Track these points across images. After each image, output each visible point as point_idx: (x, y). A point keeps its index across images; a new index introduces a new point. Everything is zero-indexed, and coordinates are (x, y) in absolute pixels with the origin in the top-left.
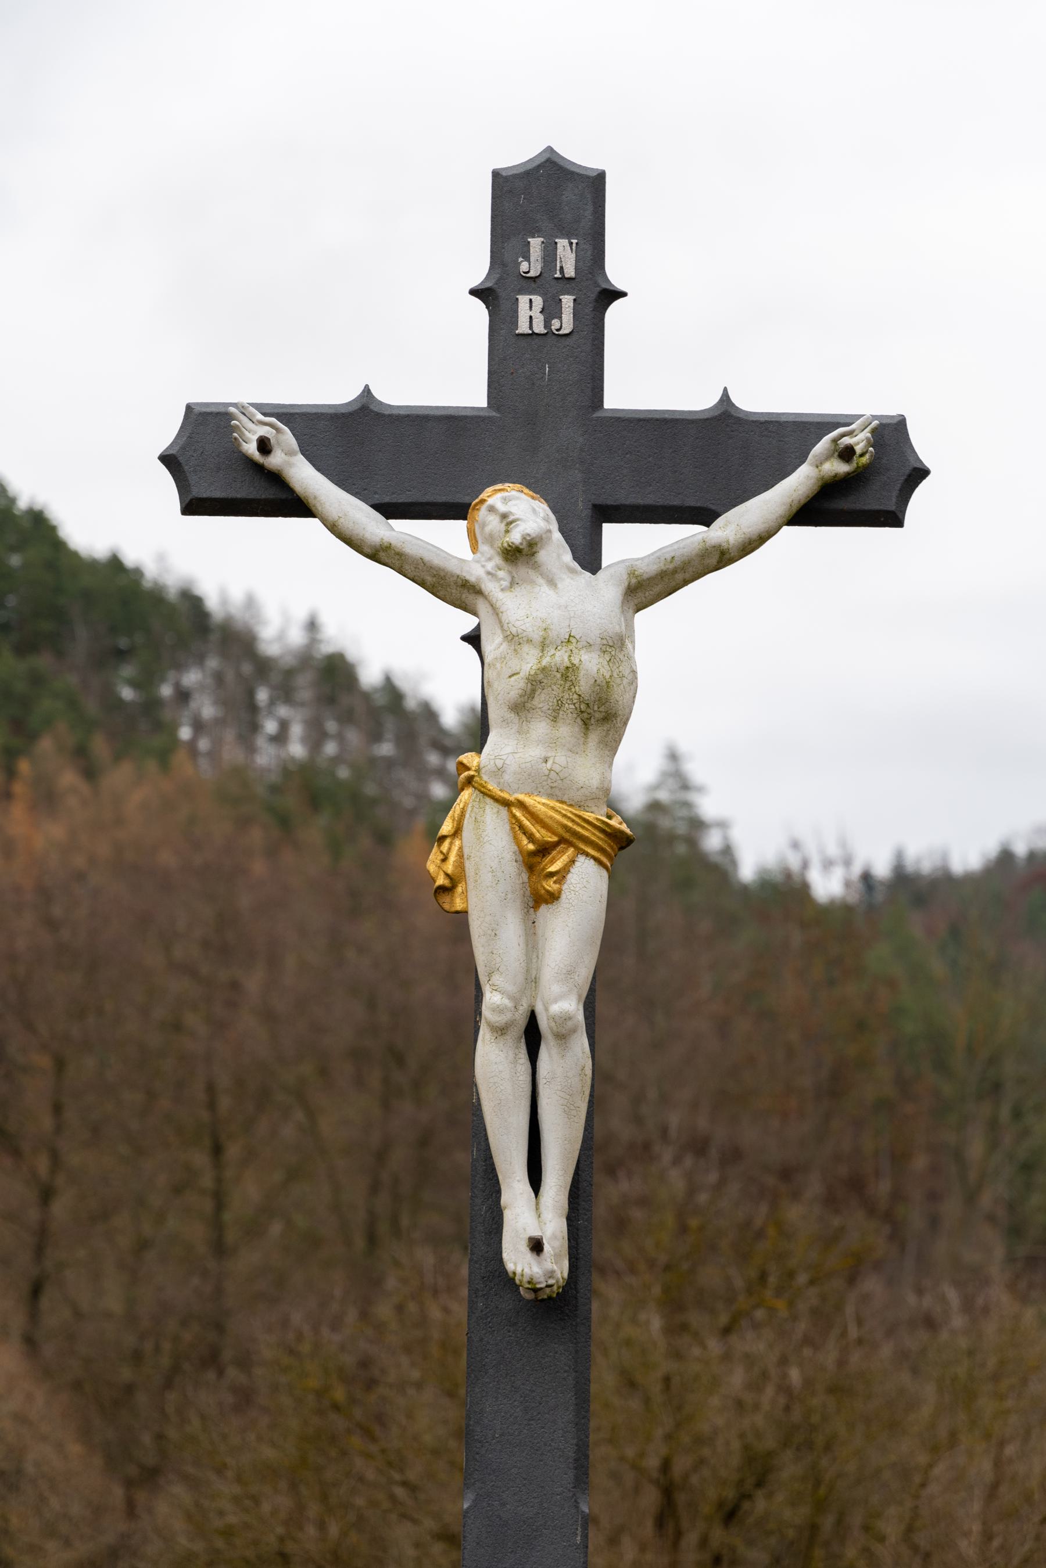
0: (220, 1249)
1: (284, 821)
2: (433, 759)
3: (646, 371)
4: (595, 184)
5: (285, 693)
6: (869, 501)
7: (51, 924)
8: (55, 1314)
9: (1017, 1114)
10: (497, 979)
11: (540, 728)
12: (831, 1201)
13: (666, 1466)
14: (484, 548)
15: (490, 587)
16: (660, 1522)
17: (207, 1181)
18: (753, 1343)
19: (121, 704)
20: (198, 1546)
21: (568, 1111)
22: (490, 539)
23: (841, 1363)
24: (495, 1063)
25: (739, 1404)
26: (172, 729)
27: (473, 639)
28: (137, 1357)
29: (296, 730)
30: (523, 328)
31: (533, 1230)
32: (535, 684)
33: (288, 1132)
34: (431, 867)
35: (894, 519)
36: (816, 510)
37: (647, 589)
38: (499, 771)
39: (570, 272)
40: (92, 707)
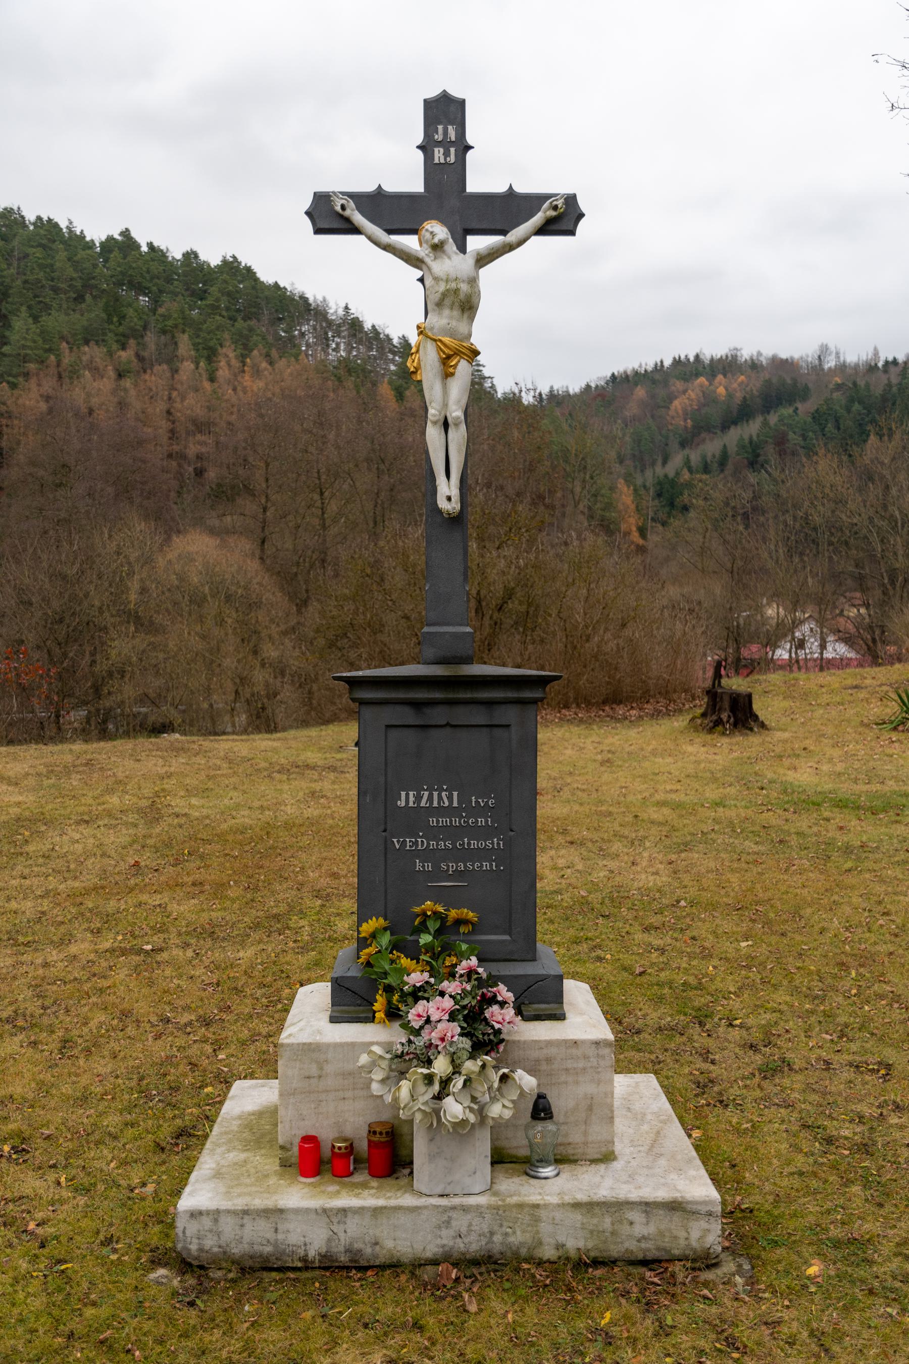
0: (324, 527)
1: (339, 379)
2: (391, 356)
3: (479, 181)
4: (462, 103)
5: (338, 334)
6: (563, 226)
7: (262, 416)
8: (269, 550)
9: (592, 478)
10: (433, 404)
11: (446, 312)
12: (534, 503)
13: (478, 593)
14: (424, 245)
15: (428, 260)
16: (477, 611)
17: (319, 504)
18: (506, 552)
19: (281, 338)
20: (324, 622)
21: (459, 451)
22: (427, 242)
23: (536, 558)
24: (433, 434)
25: (503, 572)
26: (300, 346)
27: (421, 280)
28: (298, 564)
29: (342, 347)
30: (436, 161)
31: (447, 493)
32: (444, 295)
33: (345, 487)
34: (408, 364)
35: (572, 233)
36: (546, 229)
37: (484, 259)
38: (432, 329)
39: (453, 139)
40: (270, 339)
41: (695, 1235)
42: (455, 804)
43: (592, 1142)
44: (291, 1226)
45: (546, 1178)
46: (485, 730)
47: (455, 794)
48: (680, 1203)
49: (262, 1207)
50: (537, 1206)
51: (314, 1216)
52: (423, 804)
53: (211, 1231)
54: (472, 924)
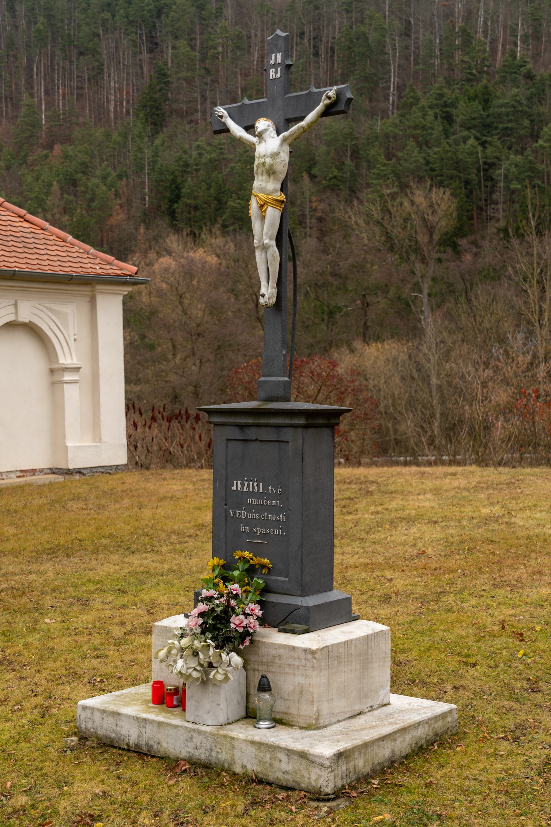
30: (271, 78)
41: (313, 777)
42: (261, 491)
43: (302, 716)
44: (123, 724)
45: (259, 728)
46: (276, 444)
47: (261, 484)
48: (306, 754)
49: (111, 710)
50: (233, 738)
51: (132, 720)
52: (245, 490)
53: (90, 719)
54: (269, 568)
